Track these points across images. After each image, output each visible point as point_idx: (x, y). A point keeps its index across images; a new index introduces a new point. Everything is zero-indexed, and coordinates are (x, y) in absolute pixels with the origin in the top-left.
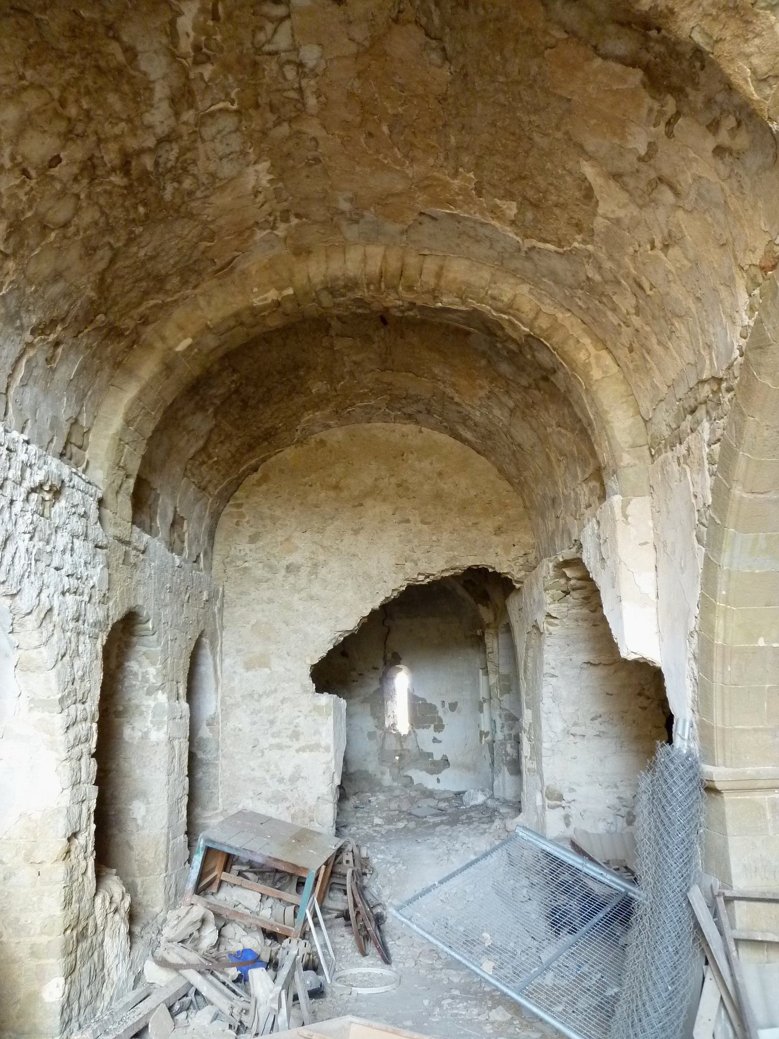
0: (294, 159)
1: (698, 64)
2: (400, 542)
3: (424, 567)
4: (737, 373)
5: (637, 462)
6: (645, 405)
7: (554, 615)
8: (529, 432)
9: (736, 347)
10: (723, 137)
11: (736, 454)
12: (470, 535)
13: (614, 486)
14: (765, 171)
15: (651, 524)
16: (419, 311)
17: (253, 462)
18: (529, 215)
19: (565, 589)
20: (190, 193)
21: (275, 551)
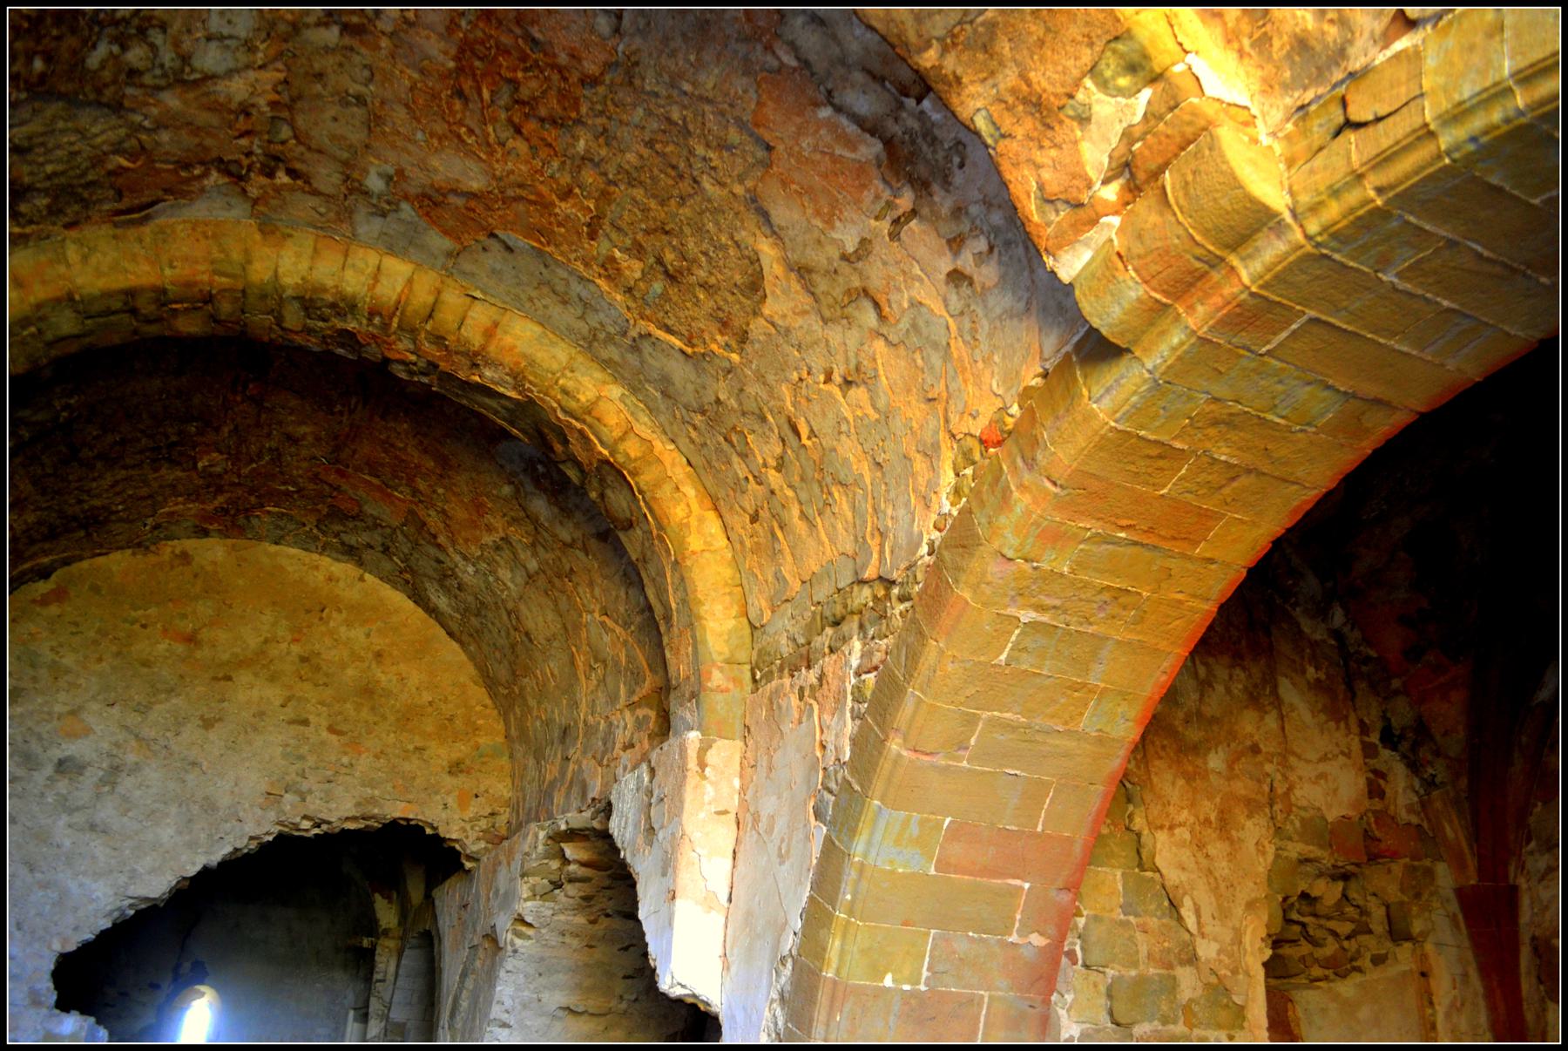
0: (324, 86)
1: (956, 160)
2: (285, 756)
3: (315, 806)
4: (920, 577)
5: (731, 686)
6: (759, 603)
7: (529, 919)
8: (550, 616)
9: (925, 540)
10: (966, 261)
11: (901, 691)
12: (407, 766)
13: (688, 716)
14: (1011, 317)
15: (737, 783)
16: (440, 379)
17: (46, 560)
18: (658, 287)
19: (555, 878)
20: (133, 73)
21: (44, 729)
